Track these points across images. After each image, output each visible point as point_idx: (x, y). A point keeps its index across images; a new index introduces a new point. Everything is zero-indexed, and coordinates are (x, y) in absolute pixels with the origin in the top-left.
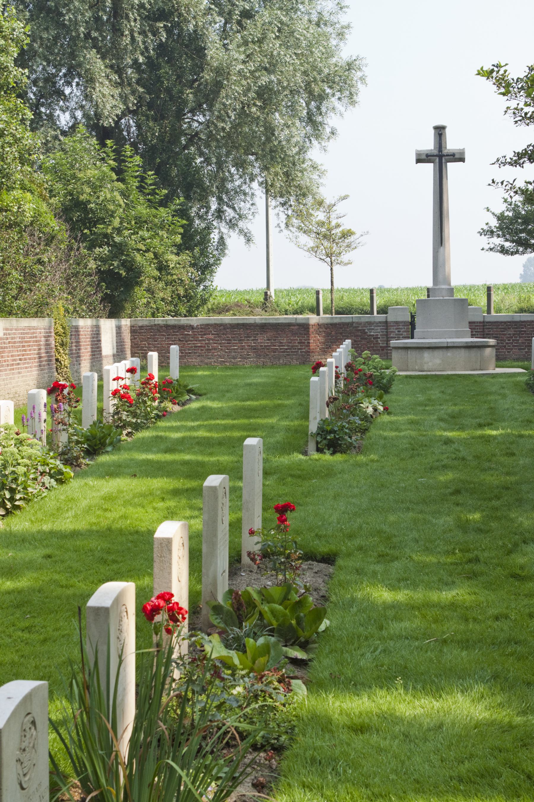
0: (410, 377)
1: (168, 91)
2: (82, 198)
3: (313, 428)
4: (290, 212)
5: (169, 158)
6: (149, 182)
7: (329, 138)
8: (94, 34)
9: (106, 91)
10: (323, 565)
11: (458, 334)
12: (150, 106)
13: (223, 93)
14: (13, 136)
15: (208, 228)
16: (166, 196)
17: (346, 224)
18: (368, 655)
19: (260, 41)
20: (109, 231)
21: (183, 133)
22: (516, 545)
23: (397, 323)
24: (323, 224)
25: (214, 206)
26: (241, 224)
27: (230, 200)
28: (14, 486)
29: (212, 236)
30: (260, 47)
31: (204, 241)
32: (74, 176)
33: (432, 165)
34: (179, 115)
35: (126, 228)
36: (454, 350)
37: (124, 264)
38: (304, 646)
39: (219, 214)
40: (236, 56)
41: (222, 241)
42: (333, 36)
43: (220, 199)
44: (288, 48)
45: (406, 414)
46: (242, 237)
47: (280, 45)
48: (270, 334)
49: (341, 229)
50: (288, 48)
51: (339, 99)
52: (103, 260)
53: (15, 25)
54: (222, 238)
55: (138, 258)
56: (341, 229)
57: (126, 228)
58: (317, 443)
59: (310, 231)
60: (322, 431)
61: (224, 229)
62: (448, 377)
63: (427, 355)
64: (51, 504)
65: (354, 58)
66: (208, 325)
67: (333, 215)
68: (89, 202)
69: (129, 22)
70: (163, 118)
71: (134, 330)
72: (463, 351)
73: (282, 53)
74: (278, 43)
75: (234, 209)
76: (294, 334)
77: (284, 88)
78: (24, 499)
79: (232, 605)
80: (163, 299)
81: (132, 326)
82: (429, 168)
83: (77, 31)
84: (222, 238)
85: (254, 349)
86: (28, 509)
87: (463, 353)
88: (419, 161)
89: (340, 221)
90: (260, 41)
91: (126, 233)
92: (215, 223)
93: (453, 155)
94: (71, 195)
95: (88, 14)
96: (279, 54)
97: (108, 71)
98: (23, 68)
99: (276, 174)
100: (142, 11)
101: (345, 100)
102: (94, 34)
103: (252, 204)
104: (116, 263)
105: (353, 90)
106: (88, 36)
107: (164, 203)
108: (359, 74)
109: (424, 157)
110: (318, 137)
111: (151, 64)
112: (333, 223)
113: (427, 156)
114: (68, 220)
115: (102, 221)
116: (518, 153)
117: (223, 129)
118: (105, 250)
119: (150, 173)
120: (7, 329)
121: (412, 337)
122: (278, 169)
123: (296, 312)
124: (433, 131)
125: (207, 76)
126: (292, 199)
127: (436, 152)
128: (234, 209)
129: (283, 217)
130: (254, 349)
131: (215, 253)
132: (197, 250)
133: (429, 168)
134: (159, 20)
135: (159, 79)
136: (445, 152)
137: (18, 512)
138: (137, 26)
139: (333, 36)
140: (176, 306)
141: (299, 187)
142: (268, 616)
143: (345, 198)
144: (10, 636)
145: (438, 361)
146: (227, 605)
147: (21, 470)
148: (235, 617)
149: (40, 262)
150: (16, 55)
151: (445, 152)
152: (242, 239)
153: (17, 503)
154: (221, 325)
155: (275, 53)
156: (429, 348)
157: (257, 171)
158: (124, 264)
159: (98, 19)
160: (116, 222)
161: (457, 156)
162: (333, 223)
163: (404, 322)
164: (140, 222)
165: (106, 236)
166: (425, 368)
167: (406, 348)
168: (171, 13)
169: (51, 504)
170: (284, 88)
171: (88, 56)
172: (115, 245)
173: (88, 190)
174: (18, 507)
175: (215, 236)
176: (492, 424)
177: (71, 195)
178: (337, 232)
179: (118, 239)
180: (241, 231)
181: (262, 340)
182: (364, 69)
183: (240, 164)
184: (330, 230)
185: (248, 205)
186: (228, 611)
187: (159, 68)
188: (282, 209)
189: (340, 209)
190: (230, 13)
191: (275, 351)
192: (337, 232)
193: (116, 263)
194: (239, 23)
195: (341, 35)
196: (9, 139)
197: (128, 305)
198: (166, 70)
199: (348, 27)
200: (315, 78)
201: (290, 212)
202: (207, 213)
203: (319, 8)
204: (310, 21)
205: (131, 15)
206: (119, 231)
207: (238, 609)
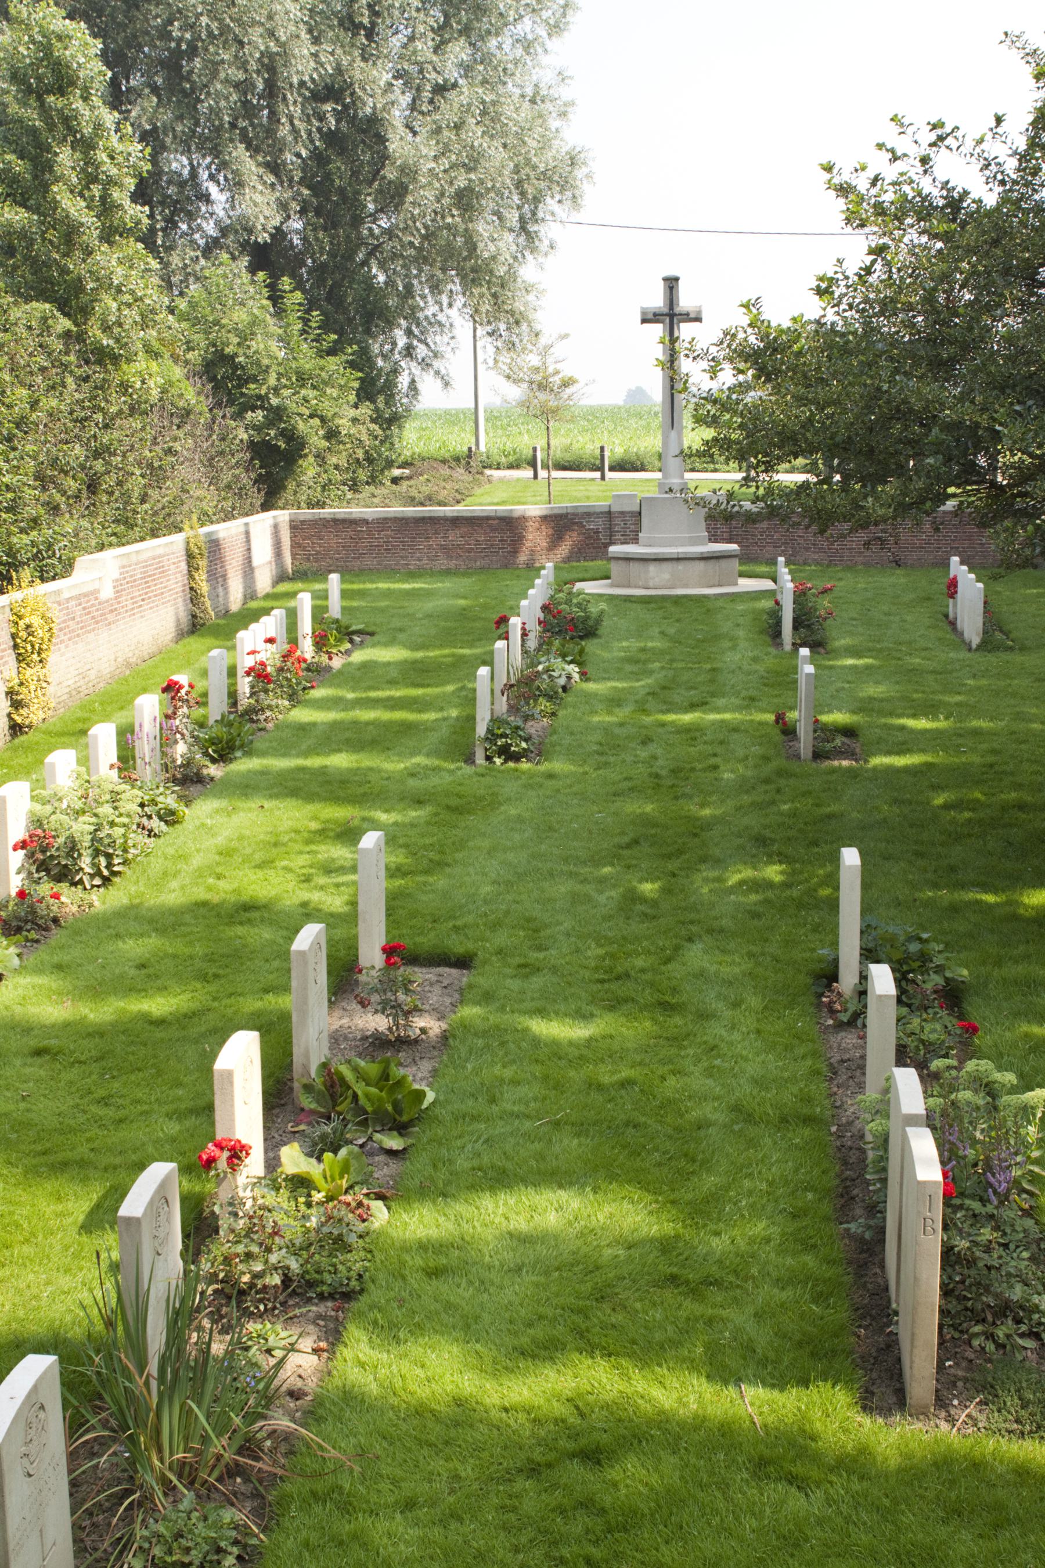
0: (628, 599)
1: (341, 191)
2: (227, 350)
3: (481, 730)
4: (499, 344)
5: (343, 279)
6: (314, 325)
7: (546, 254)
8: (242, 123)
9: (259, 198)
10: (454, 971)
11: (694, 542)
12: (318, 213)
13: (410, 198)
14: (132, 292)
15: (395, 371)
16: (335, 342)
17: (567, 371)
18: (469, 1147)
19: (457, 127)
20: (263, 392)
21: (361, 242)
22: (677, 948)
23: (622, 513)
24: (537, 370)
25: (402, 341)
26: (436, 364)
27: (422, 333)
28: (111, 851)
29: (400, 379)
30: (457, 135)
31: (389, 389)
32: (216, 323)
33: (660, 326)
34: (357, 221)
35: (285, 386)
36: (687, 563)
37: (283, 433)
38: (402, 1129)
39: (409, 351)
40: (424, 151)
41: (413, 384)
42: (554, 115)
43: (409, 332)
44: (492, 137)
45: (609, 679)
46: (439, 381)
47: (484, 132)
48: (464, 530)
49: (560, 376)
50: (492, 137)
51: (560, 202)
52: (258, 428)
53: (131, 149)
54: (413, 381)
55: (301, 426)
56: (560, 376)
57: (285, 386)
58: (486, 750)
59: (521, 380)
60: (492, 736)
61: (416, 370)
62: (677, 600)
63: (653, 568)
64: (156, 865)
65: (578, 149)
66: (386, 519)
67: (550, 360)
68: (236, 355)
69: (287, 106)
70: (334, 226)
71: (295, 527)
72: (697, 562)
73: (485, 145)
74: (479, 131)
75: (427, 345)
76: (493, 529)
77: (488, 190)
78: (123, 864)
79: (324, 1084)
80: (336, 467)
81: (291, 521)
82: (657, 330)
83: (221, 120)
84: (413, 381)
85: (443, 547)
86: (129, 873)
87: (701, 566)
88: (644, 321)
89: (559, 366)
90: (457, 127)
91: (286, 392)
92: (402, 363)
93: (688, 314)
94: (214, 345)
95: (235, 97)
96: (481, 145)
97: (261, 170)
98: (143, 205)
99: (481, 296)
100: (303, 91)
101: (568, 203)
102: (242, 123)
103: (453, 338)
104: (272, 433)
105: (577, 193)
106: (233, 125)
107: (332, 352)
108: (584, 170)
109: (650, 316)
110: (533, 250)
111: (317, 156)
112: (550, 370)
113: (655, 315)
114: (212, 379)
115: (254, 379)
116: (708, 442)
117: (411, 244)
118: (259, 416)
119: (315, 313)
120: (124, 567)
121: (635, 540)
122: (484, 290)
123: (511, 467)
124: (661, 284)
125: (390, 173)
126: (502, 326)
127: (666, 310)
128: (427, 345)
129: (491, 350)
130: (443, 547)
131: (405, 400)
132: (381, 399)
133: (657, 330)
134: (325, 100)
135: (328, 177)
136: (677, 310)
137: (116, 880)
138: (297, 111)
139: (554, 115)
140: (354, 472)
141: (512, 313)
142: (362, 1101)
143: (566, 336)
144: (85, 1112)
145: (667, 576)
146: (319, 1083)
147: (118, 831)
148: (328, 1097)
149: (169, 451)
150: (133, 188)
151: (677, 310)
152: (439, 383)
153: (116, 869)
154: (403, 519)
155: (476, 144)
156: (655, 560)
157: (457, 288)
158: (283, 433)
159: (246, 103)
160: (272, 381)
161: (692, 316)
162: (550, 370)
163: (632, 512)
164: (302, 379)
165: (259, 397)
166: (651, 584)
167: (628, 559)
168: (342, 90)
169: (156, 865)
170: (488, 190)
171: (234, 154)
172: (271, 409)
173: (236, 340)
174: (119, 873)
175: (403, 381)
176: (706, 703)
177: (214, 345)
178: (556, 380)
179: (275, 401)
180: (437, 373)
181: (454, 536)
182: (590, 163)
183: (436, 288)
184: (546, 378)
185: (446, 339)
186: (319, 1091)
187: (329, 161)
188: (489, 339)
189: (558, 351)
190: (418, 89)
191: (469, 551)
192: (556, 380)
193: (272, 433)
194: (431, 101)
195: (563, 114)
196: (127, 298)
197: (291, 485)
198: (338, 165)
199: (572, 104)
200: (528, 175)
201: (499, 344)
202: (392, 350)
203: (535, 78)
204: (523, 96)
205: (289, 96)
206: (276, 390)
207: (332, 1086)
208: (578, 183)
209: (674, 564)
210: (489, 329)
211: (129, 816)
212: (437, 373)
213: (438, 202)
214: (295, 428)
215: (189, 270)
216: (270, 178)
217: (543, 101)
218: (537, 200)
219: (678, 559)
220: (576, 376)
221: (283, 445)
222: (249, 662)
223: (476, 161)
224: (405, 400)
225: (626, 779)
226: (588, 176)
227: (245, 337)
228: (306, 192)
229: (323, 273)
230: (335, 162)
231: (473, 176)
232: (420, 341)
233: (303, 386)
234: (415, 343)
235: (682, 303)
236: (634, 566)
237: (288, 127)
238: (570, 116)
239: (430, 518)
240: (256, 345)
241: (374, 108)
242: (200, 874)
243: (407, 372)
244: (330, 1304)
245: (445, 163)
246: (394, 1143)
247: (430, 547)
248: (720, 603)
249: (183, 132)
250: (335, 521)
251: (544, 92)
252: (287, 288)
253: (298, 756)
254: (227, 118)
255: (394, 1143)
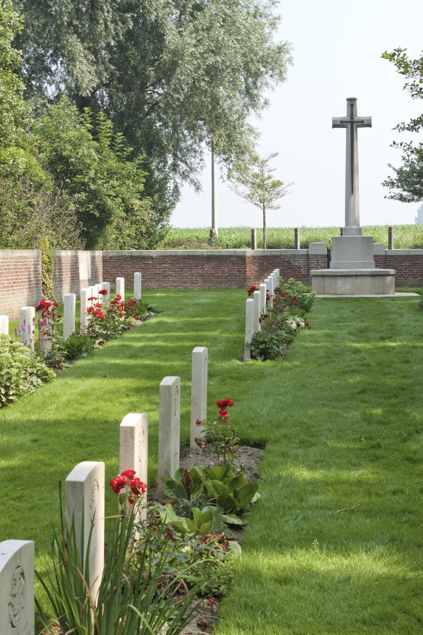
0: (326, 299)
1: (134, 68)
2: (64, 153)
4: (231, 166)
5: (134, 122)
6: (119, 141)
7: (262, 107)
8: (76, 22)
9: (84, 68)
11: (365, 265)
13: (178, 70)
14: (10, 103)
15: (166, 179)
16: (132, 152)
17: (276, 177)
18: (291, 521)
19: (208, 29)
20: (86, 180)
21: (146, 102)
23: (316, 256)
26: (192, 175)
27: (183, 156)
28: (8, 384)
29: (168, 185)
30: (208, 34)
31: (162, 189)
32: (58, 136)
33: (344, 130)
34: (143, 88)
35: (100, 178)
36: (362, 278)
37: (97, 207)
38: (240, 514)
39: (174, 168)
40: (189, 41)
42: (267, 25)
44: (230, 35)
46: (193, 186)
47: (224, 32)
48: (214, 264)
49: (272, 180)
50: (230, 35)
51: (271, 76)
52: (81, 204)
53: (12, 15)
54: (176, 187)
55: (109, 202)
56: (272, 180)
57: (100, 178)
58: (252, 351)
59: (247, 182)
61: (178, 180)
62: (357, 299)
63: (340, 281)
64: (37, 399)
65: (283, 43)
66: (164, 256)
67: (266, 169)
68: (70, 157)
69: (103, 13)
70: (130, 90)
71: (106, 260)
73: (226, 39)
74: (222, 31)
75: (186, 163)
76: (234, 264)
79: (182, 481)
81: (104, 257)
82: (343, 132)
83: (61, 19)
84: (176, 187)
85: (202, 275)
86: (19, 402)
88: (334, 126)
89: (271, 174)
91: (100, 182)
92: (171, 175)
93: (362, 122)
94: (56, 151)
96: (223, 39)
97: (86, 52)
98: (18, 49)
99: (220, 136)
101: (276, 77)
102: (76, 22)
103: (201, 160)
104: (91, 206)
105: (282, 69)
106: (70, 24)
107: (130, 158)
108: (287, 56)
109: (339, 123)
110: (254, 106)
112: (266, 176)
113: (341, 122)
114: (53, 171)
115: (80, 172)
116: (414, 121)
117: (178, 99)
118: (83, 196)
119: (119, 134)
121: (328, 268)
124: (346, 103)
125: (166, 57)
127: (348, 119)
129: (225, 170)
130: (202, 275)
132: (156, 196)
133: (343, 132)
134: (127, 11)
135: (127, 59)
136: (355, 119)
137: (11, 405)
138: (109, 16)
140: (139, 240)
141: (239, 146)
143: (275, 155)
145: (349, 287)
147: (14, 371)
148: (185, 491)
149: (30, 204)
150: (12, 39)
151: (355, 119)
152: (193, 187)
153: (10, 398)
154: (175, 256)
155: (220, 39)
158: (97, 207)
160: (92, 173)
162: (266, 176)
164: (111, 174)
165: (83, 184)
166: (339, 292)
167: (323, 276)
169: (37, 399)
171: (70, 40)
172: (91, 192)
173: (69, 147)
175: (171, 185)
176: (391, 337)
177: (56, 151)
179: (93, 187)
180: (192, 181)
181: (208, 268)
182: (291, 52)
183: (192, 128)
184: (263, 181)
185: (197, 161)
187: (127, 50)
188: (224, 164)
189: (271, 164)
191: (218, 277)
193: (91, 206)
194: (192, 14)
195: (273, 25)
198: (132, 51)
199: (279, 18)
201: (231, 166)
202: (164, 166)
204: (248, 13)
206: (94, 180)
208: (283, 62)
209: (354, 278)
210: (224, 157)
211: (21, 362)
212: (192, 181)
213: (196, 73)
214: (105, 204)
215: (39, 111)
216: (92, 57)
217: (261, 16)
218: (257, 75)
219: (356, 276)
220: (282, 181)
221: (97, 214)
222: (89, 304)
223: (220, 49)
224: (171, 198)
225: (348, 367)
226: (290, 60)
227: (75, 146)
228: (113, 67)
229: (122, 118)
230: (131, 50)
231: (218, 58)
232: (181, 161)
233: (111, 178)
234: (179, 162)
235: (358, 115)
236: (327, 281)
237: (102, 27)
238: (278, 26)
239: (193, 256)
240: (83, 150)
241: (157, 16)
242: (68, 403)
243: (172, 181)
244: (206, 601)
245: (201, 49)
246: (235, 520)
247: (192, 275)
248: (386, 301)
249: (39, 26)
250: (132, 257)
251: (261, 9)
252: (102, 118)
253: (124, 358)
254: (66, 18)
255: (235, 520)
